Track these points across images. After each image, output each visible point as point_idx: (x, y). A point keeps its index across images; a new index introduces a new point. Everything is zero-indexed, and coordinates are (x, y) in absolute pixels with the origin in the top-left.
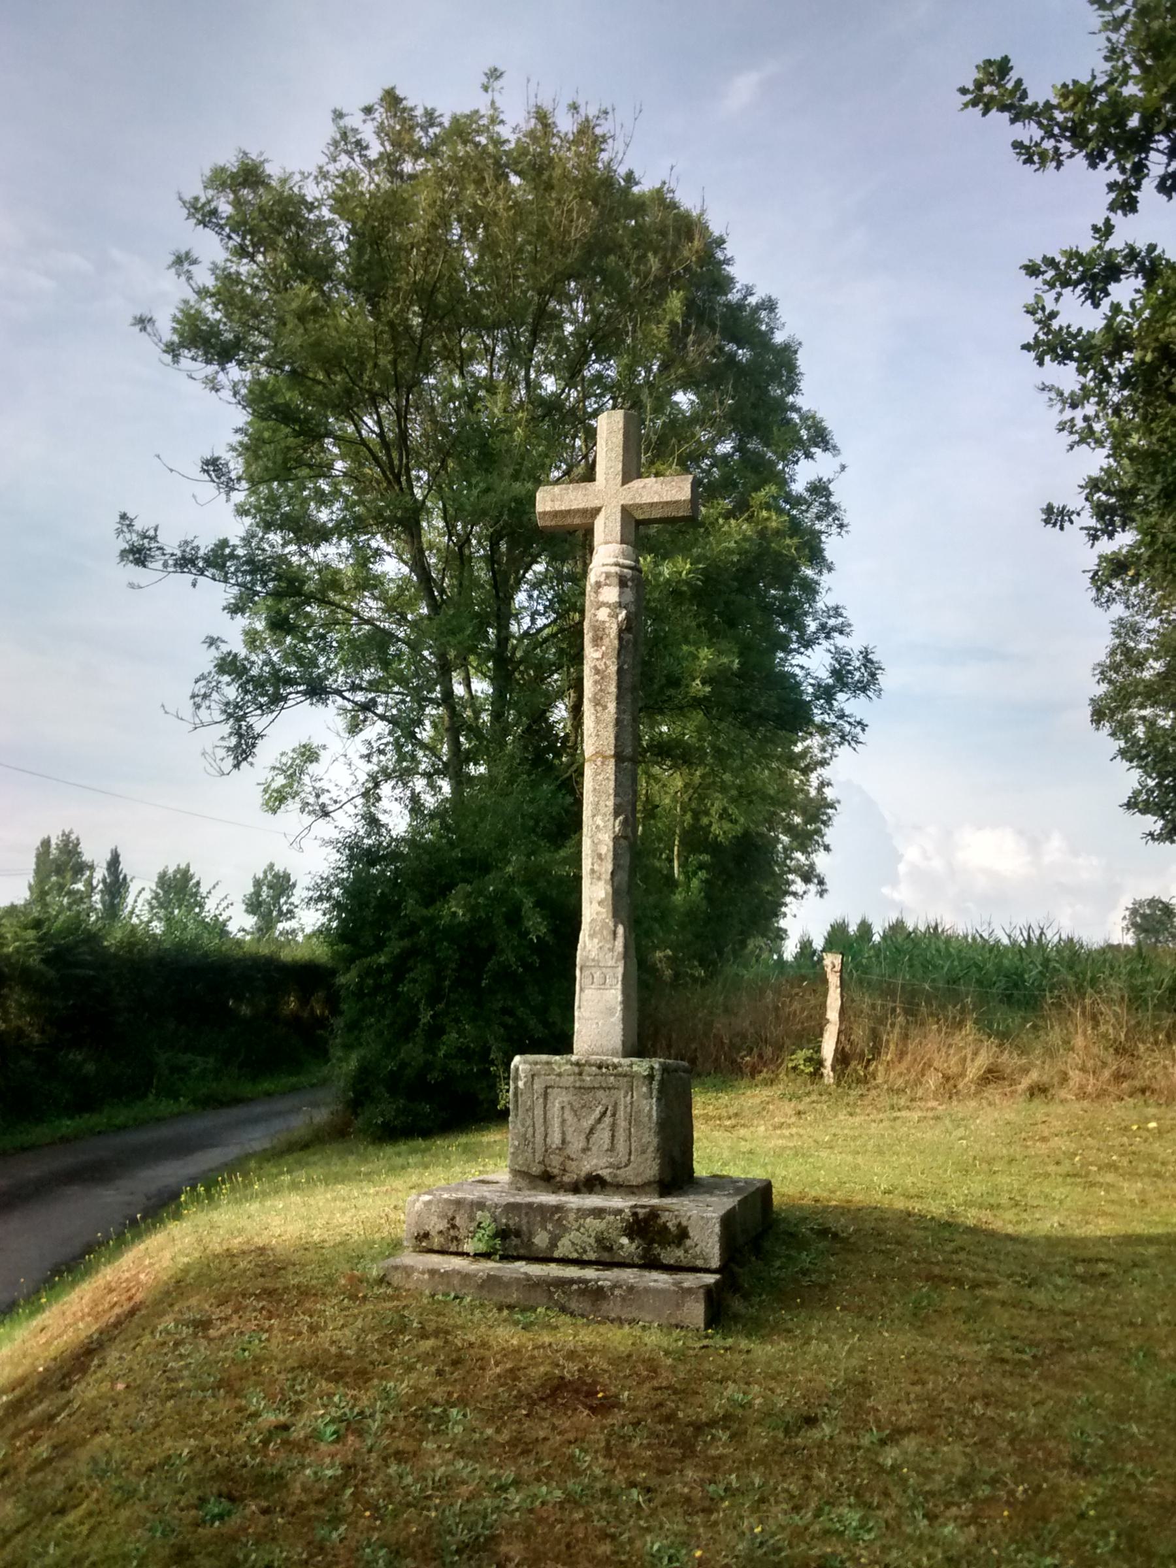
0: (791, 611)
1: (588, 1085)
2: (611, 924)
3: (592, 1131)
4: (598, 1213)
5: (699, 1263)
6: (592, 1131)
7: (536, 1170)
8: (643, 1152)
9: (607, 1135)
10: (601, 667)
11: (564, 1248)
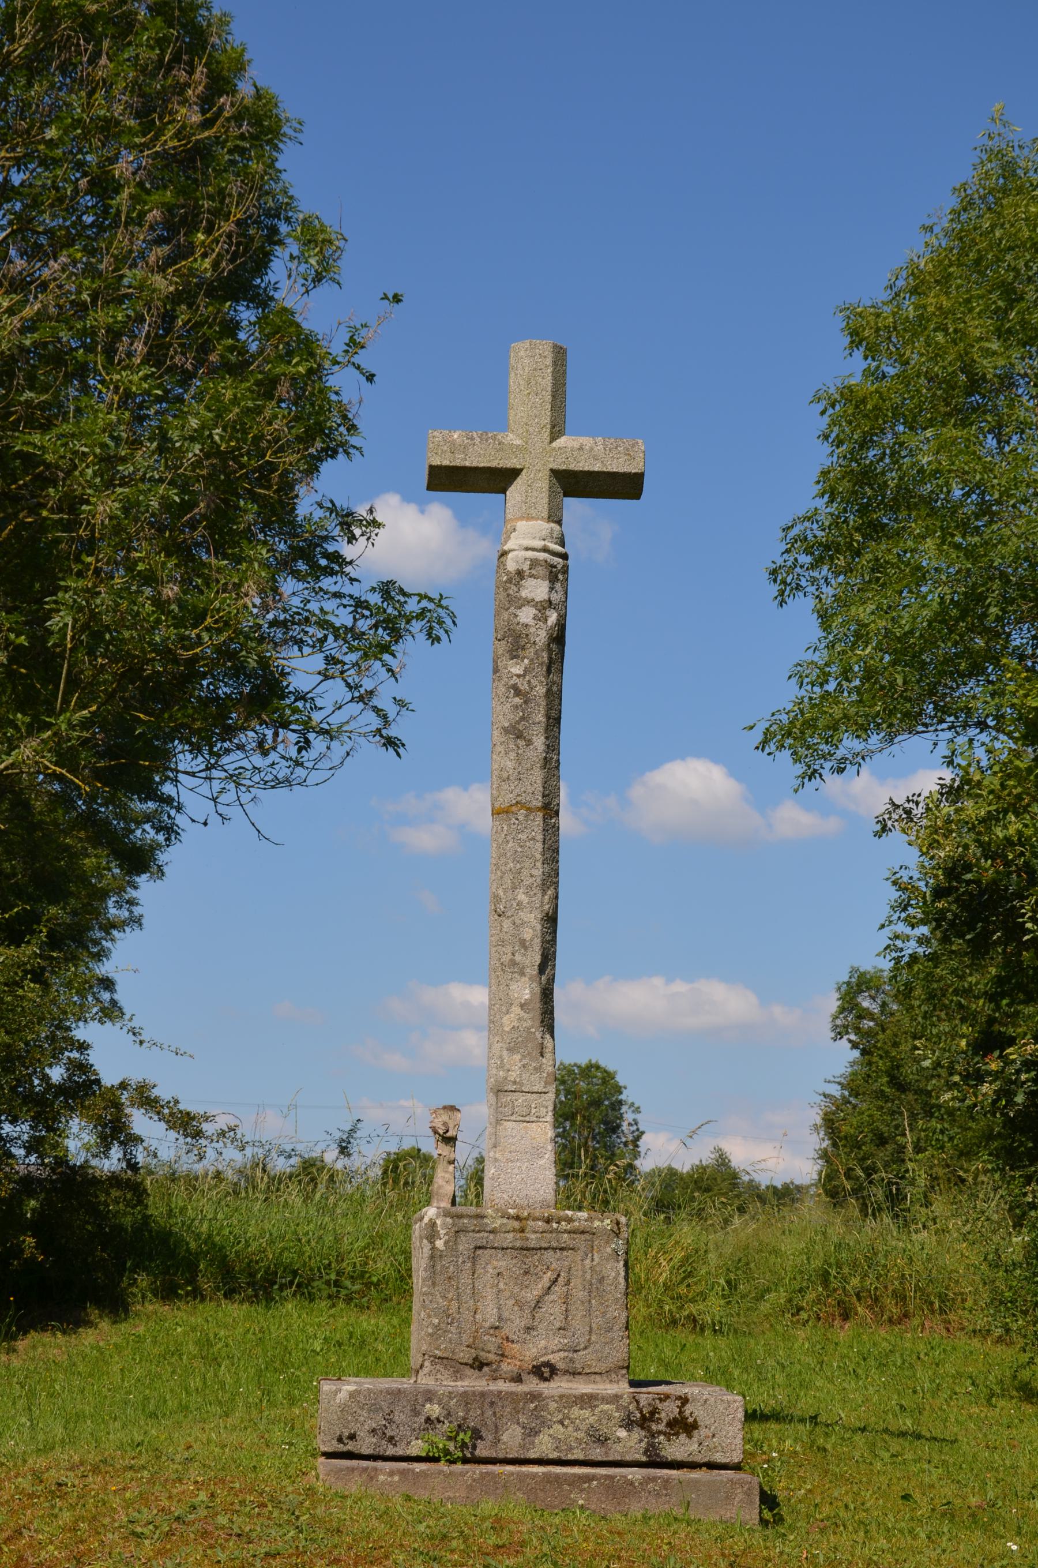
2: (539, 1035)
4: (588, 1401)
5: (719, 1458)
7: (465, 1355)
8: (610, 1330)
9: (558, 1309)
10: (524, 687)
11: (544, 1446)
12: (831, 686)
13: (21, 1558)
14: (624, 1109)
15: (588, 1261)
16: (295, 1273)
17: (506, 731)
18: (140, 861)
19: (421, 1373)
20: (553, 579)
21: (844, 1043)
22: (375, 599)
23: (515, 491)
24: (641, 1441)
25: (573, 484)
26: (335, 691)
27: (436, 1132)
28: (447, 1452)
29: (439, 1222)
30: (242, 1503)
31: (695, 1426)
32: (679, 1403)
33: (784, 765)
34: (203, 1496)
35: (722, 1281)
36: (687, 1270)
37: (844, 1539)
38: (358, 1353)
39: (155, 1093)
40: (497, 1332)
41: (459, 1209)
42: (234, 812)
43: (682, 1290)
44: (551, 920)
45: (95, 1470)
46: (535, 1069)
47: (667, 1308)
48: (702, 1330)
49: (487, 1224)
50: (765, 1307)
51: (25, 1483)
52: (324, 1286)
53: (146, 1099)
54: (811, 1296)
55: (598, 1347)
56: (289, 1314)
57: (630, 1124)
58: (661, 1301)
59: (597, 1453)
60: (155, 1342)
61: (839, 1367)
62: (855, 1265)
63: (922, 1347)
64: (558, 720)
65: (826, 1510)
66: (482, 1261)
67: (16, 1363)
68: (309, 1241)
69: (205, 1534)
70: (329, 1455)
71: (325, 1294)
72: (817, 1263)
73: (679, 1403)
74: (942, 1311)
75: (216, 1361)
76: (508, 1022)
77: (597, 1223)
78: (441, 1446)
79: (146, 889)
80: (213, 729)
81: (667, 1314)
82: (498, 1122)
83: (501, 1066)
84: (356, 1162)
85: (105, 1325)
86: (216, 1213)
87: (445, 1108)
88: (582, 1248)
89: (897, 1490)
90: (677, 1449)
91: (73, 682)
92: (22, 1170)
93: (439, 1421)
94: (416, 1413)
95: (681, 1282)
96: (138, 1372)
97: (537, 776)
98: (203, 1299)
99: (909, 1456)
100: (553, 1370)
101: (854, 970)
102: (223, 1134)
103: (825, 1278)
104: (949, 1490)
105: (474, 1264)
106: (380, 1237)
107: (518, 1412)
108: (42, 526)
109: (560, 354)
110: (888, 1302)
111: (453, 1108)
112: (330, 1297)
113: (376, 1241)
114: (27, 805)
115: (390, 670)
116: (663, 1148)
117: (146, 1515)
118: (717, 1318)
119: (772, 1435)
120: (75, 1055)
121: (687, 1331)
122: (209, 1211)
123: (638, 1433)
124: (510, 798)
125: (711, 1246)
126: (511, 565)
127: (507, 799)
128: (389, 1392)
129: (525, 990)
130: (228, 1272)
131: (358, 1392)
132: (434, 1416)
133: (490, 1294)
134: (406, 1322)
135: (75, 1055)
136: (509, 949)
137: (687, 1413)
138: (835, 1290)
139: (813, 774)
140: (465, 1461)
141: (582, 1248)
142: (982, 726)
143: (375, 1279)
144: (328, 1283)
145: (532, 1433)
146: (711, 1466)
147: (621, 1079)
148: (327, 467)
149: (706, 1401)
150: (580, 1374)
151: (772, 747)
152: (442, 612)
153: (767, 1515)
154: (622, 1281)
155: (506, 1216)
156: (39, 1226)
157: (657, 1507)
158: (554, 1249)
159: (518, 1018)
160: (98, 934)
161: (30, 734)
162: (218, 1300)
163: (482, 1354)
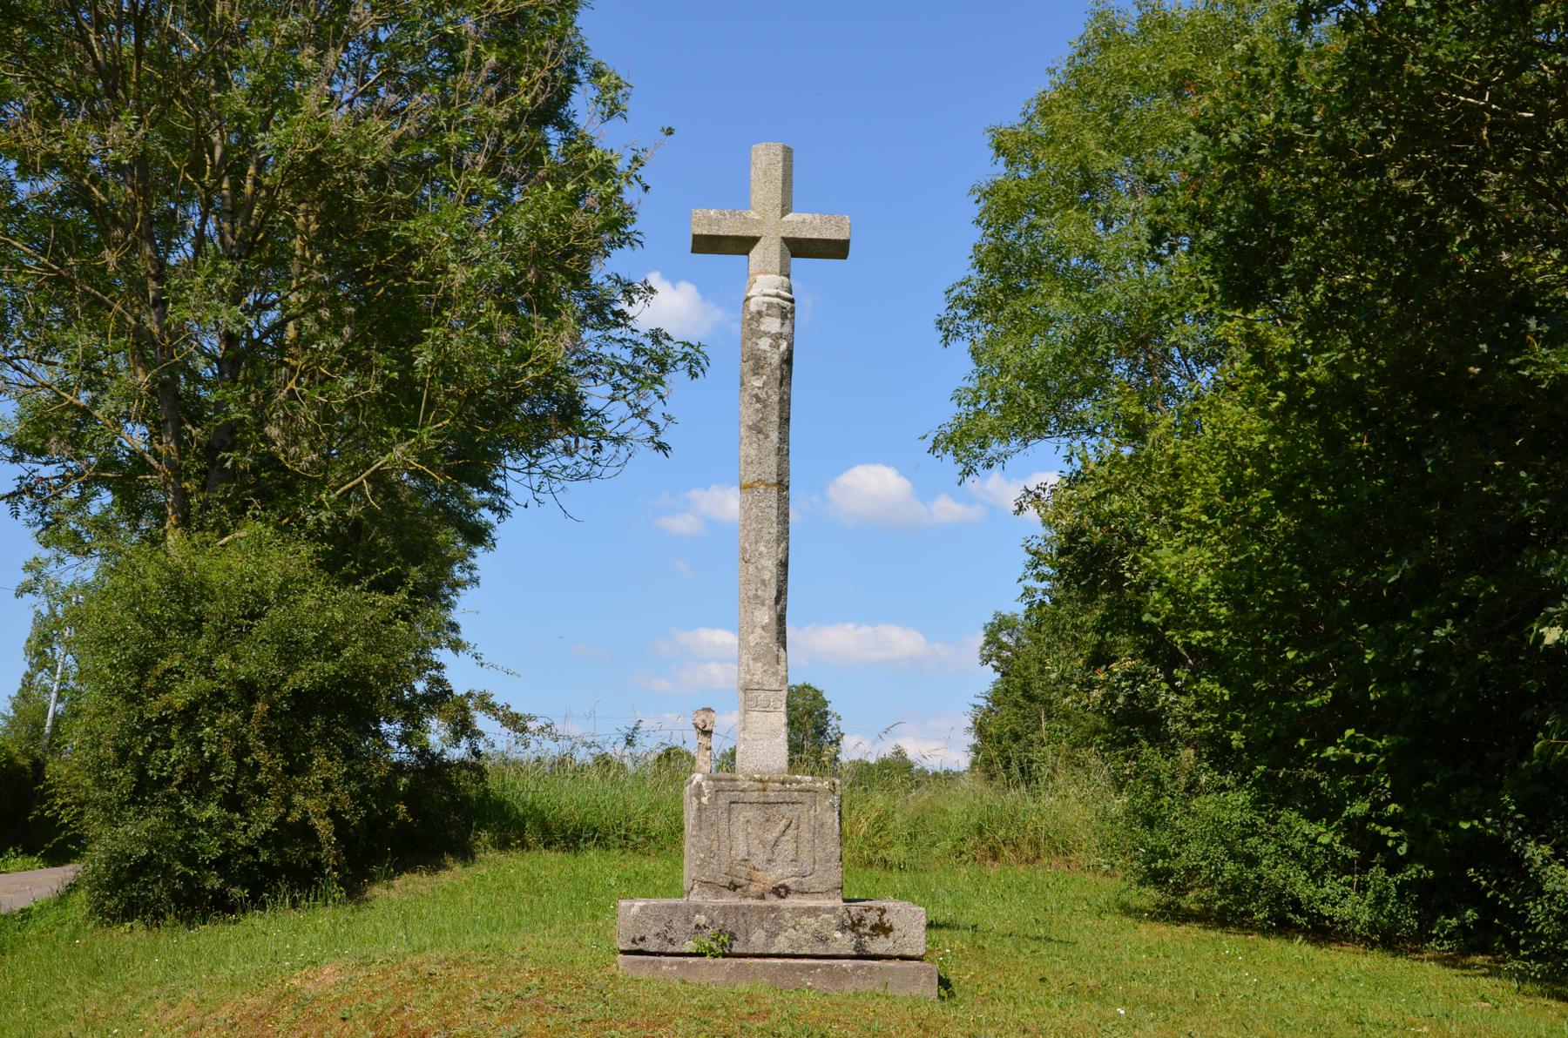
0: (1285, 141)
3: (776, 843)
4: (813, 912)
5: (908, 952)
6: (776, 843)
7: (724, 881)
10: (763, 396)
11: (781, 945)
12: (981, 406)
13: (404, 1026)
16: (595, 830)
17: (750, 428)
18: (478, 535)
20: (784, 316)
21: (989, 668)
22: (648, 343)
23: (756, 253)
25: (798, 248)
26: (619, 410)
28: (711, 950)
30: (564, 985)
31: (891, 929)
33: (949, 464)
34: (535, 981)
36: (880, 825)
37: (1000, 1008)
38: (640, 884)
39: (492, 700)
41: (720, 774)
42: (547, 498)
43: (876, 840)
44: (784, 565)
45: (456, 964)
50: (936, 852)
51: (406, 974)
53: (487, 706)
59: (820, 950)
60: (494, 879)
62: (1001, 820)
63: (1050, 879)
64: (788, 420)
65: (985, 989)
67: (394, 895)
69: (538, 1007)
70: (625, 952)
72: (974, 820)
74: (1065, 854)
75: (539, 893)
76: (753, 639)
79: (482, 558)
80: (532, 439)
81: (867, 857)
82: (746, 712)
83: (748, 672)
84: (639, 750)
85: (458, 868)
89: (1036, 975)
90: (878, 945)
91: (431, 403)
92: (395, 757)
94: (689, 922)
96: (482, 901)
97: (773, 461)
98: (529, 849)
99: (1043, 952)
100: (788, 891)
101: (997, 614)
102: (542, 729)
104: (1073, 975)
108: (408, 290)
109: (788, 153)
110: (1025, 847)
111: (709, 710)
113: (653, 807)
114: (395, 495)
115: (661, 397)
116: (858, 745)
117: (494, 994)
120: (434, 672)
122: (532, 785)
123: (849, 935)
124: (754, 477)
126: (753, 307)
127: (750, 478)
129: (765, 616)
131: (646, 907)
133: (741, 837)
134: (678, 865)
135: (434, 672)
136: (753, 586)
139: (968, 471)
140: (725, 956)
142: (1091, 433)
145: (773, 935)
146: (903, 958)
147: (826, 696)
148: (616, 253)
151: (939, 452)
152: (700, 356)
153: (943, 993)
155: (752, 779)
156: (410, 797)
157: (864, 986)
159: (761, 637)
160: (446, 591)
161: (400, 441)
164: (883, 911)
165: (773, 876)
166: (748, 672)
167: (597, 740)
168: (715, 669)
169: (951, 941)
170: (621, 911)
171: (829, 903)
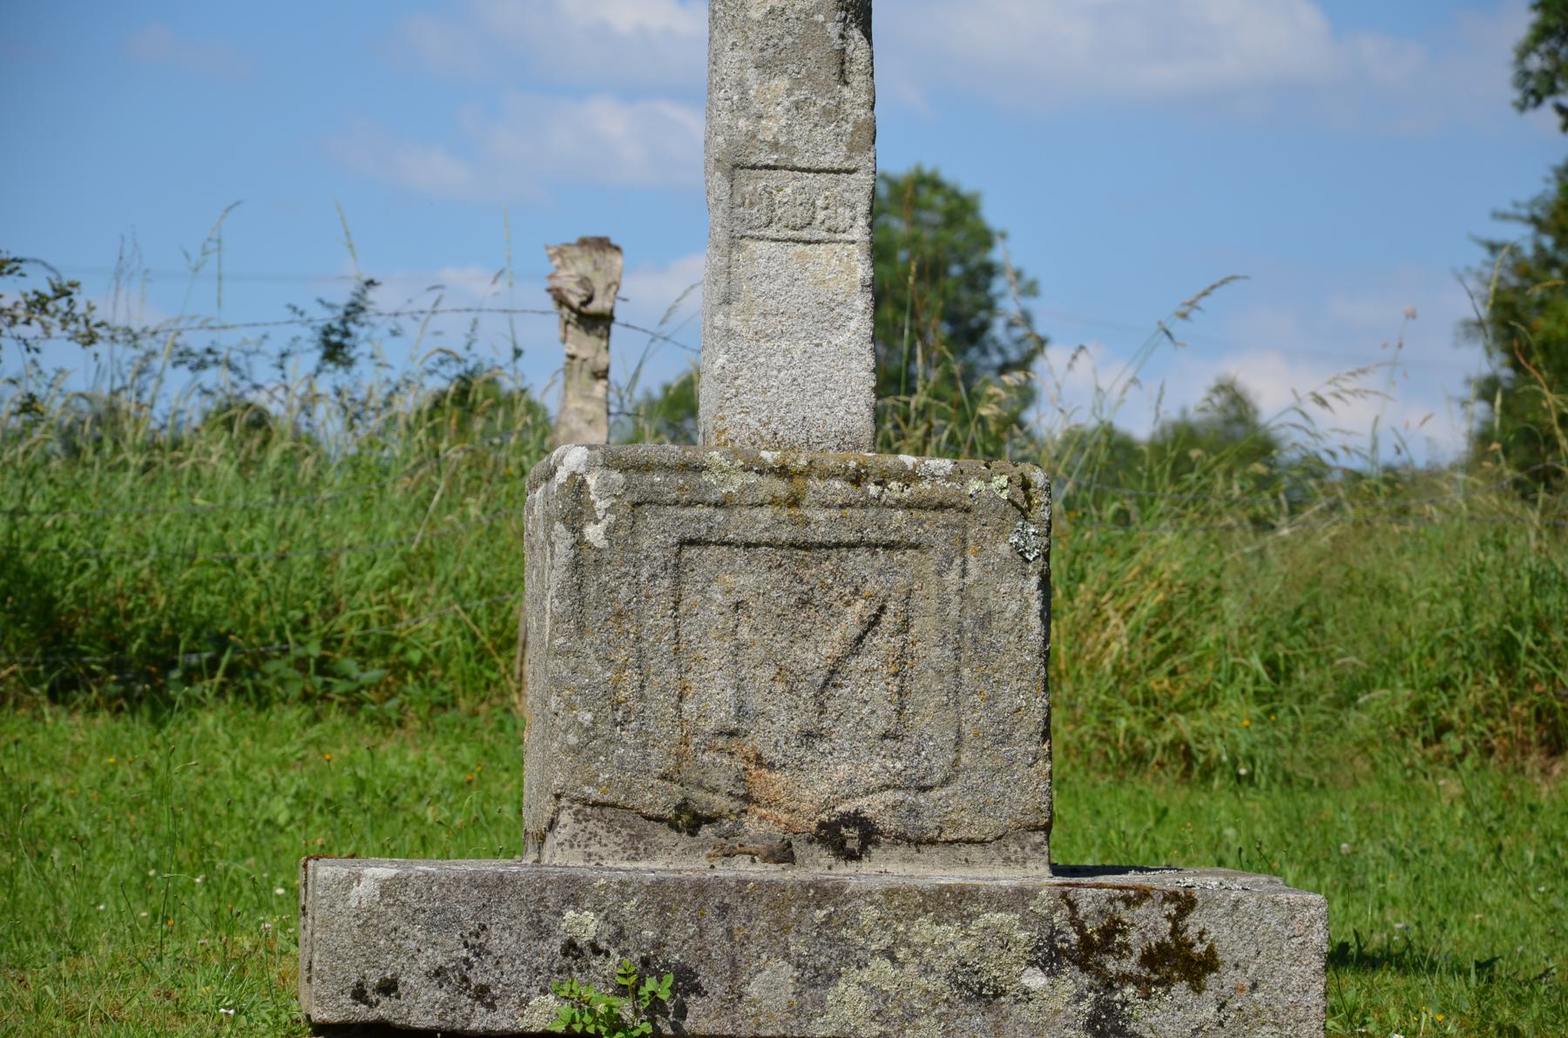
1: (819, 534)
2: (833, 30)
3: (833, 676)
4: (953, 903)
6: (833, 676)
7: (661, 799)
8: (1005, 739)
9: (880, 690)
14: (998, 285)
15: (953, 576)
16: (221, 642)
19: (551, 841)
24: (1080, 997)
27: (561, 301)
29: (592, 481)
31: (1209, 963)
32: (1171, 909)
35: (1256, 662)
36: (1168, 637)
38: (378, 818)
40: (734, 742)
41: (648, 449)
43: (1158, 682)
46: (825, 112)
47: (1122, 724)
48: (1207, 775)
49: (708, 487)
50: (1358, 723)
52: (292, 673)
54: (1472, 695)
55: (975, 778)
56: (207, 739)
57: (1011, 325)
58: (1107, 708)
61: (1540, 861)
66: (698, 576)
68: (254, 567)
71: (295, 690)
72: (1486, 620)
73: (1171, 909)
77: (974, 486)
78: (601, 1008)
81: (1129, 737)
82: (735, 241)
84: (366, 378)
86: (24, 498)
87: (583, 243)
88: (940, 545)
93: (597, 951)
94: (541, 931)
95: (1157, 664)
100: (869, 834)
103: (1506, 652)
105: (678, 582)
106: (429, 557)
107: (785, 930)
111: (602, 244)
112: (306, 698)
116: (1091, 381)
118: (1243, 748)
119: (1387, 999)
121: (1168, 779)
123: (1073, 980)
125: (1228, 580)
128: (475, 882)
130: (58, 639)
131: (402, 882)
132: (583, 940)
133: (716, 653)
137: (1191, 933)
138: (1530, 683)
141: (940, 545)
143: (415, 656)
144: (301, 664)
147: (992, 215)
149: (1236, 904)
150: (932, 842)
154: (1035, 622)
158: (872, 546)
162: (35, 706)
163: (697, 794)
164: (1185, 903)
165: (819, 787)
166: (743, 106)
167: (226, 342)
168: (610, 120)
169: (1407, 1009)
170: (317, 899)
171: (1006, 877)
